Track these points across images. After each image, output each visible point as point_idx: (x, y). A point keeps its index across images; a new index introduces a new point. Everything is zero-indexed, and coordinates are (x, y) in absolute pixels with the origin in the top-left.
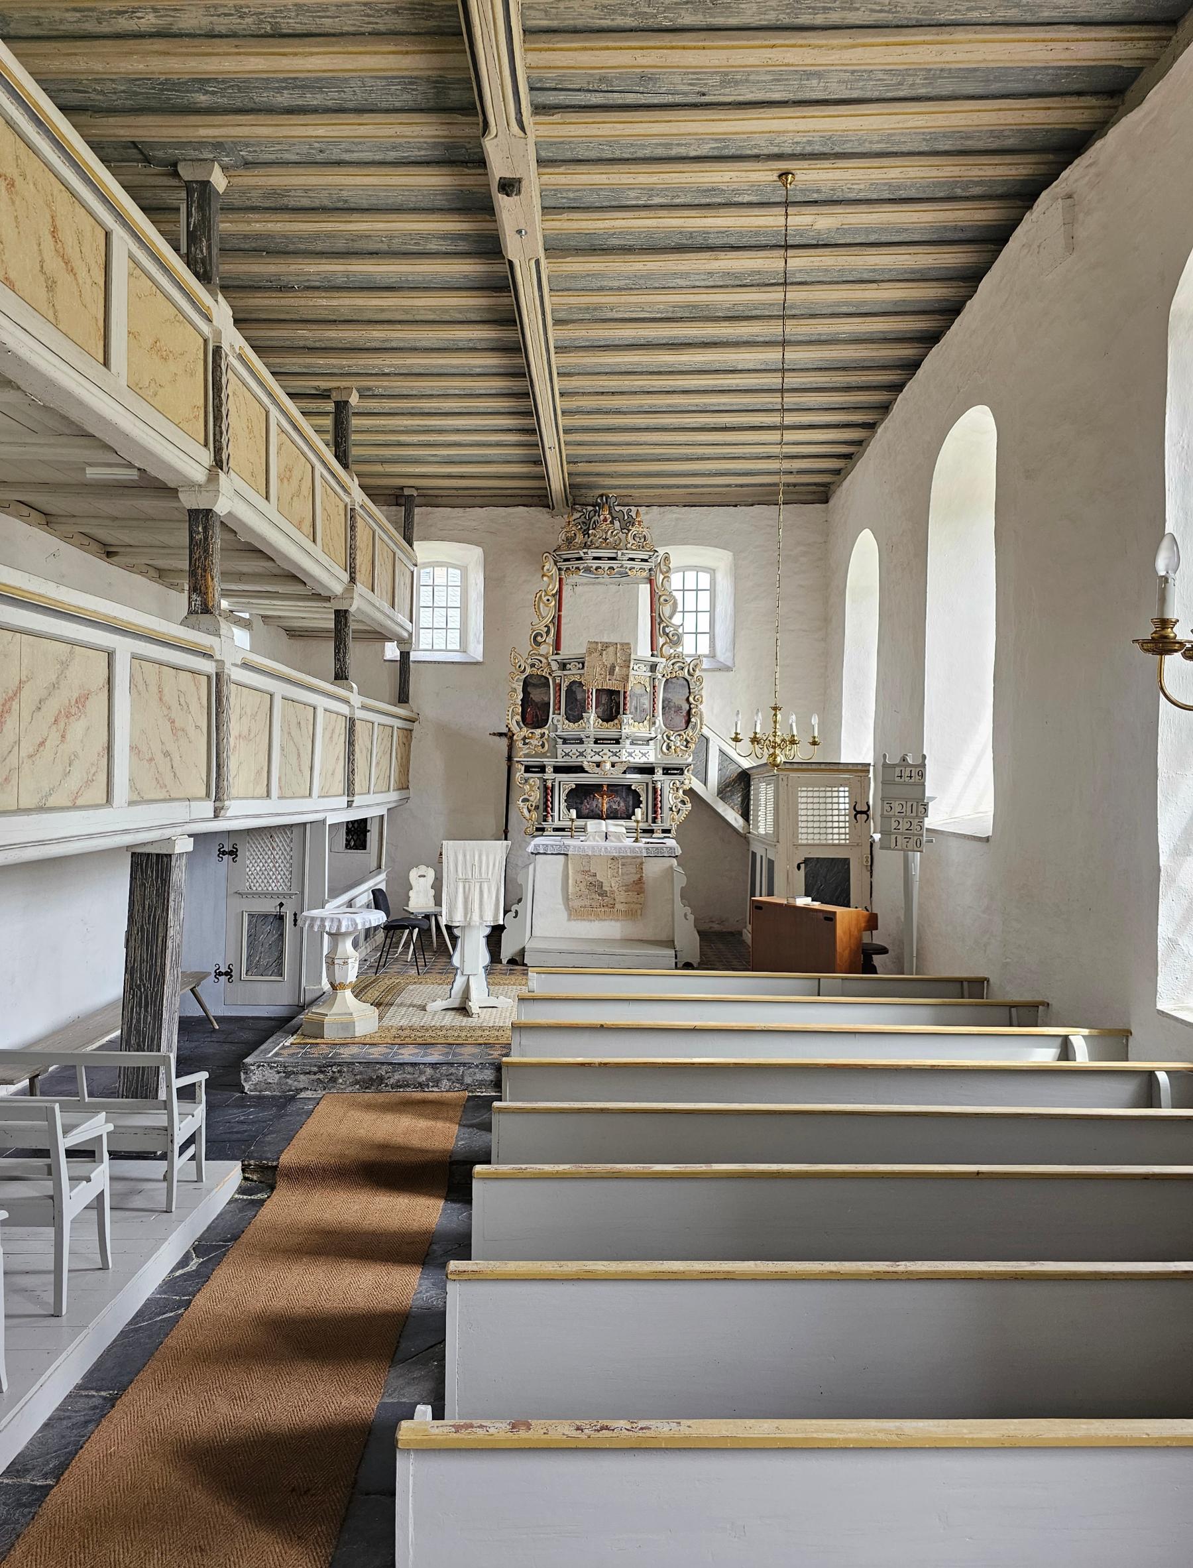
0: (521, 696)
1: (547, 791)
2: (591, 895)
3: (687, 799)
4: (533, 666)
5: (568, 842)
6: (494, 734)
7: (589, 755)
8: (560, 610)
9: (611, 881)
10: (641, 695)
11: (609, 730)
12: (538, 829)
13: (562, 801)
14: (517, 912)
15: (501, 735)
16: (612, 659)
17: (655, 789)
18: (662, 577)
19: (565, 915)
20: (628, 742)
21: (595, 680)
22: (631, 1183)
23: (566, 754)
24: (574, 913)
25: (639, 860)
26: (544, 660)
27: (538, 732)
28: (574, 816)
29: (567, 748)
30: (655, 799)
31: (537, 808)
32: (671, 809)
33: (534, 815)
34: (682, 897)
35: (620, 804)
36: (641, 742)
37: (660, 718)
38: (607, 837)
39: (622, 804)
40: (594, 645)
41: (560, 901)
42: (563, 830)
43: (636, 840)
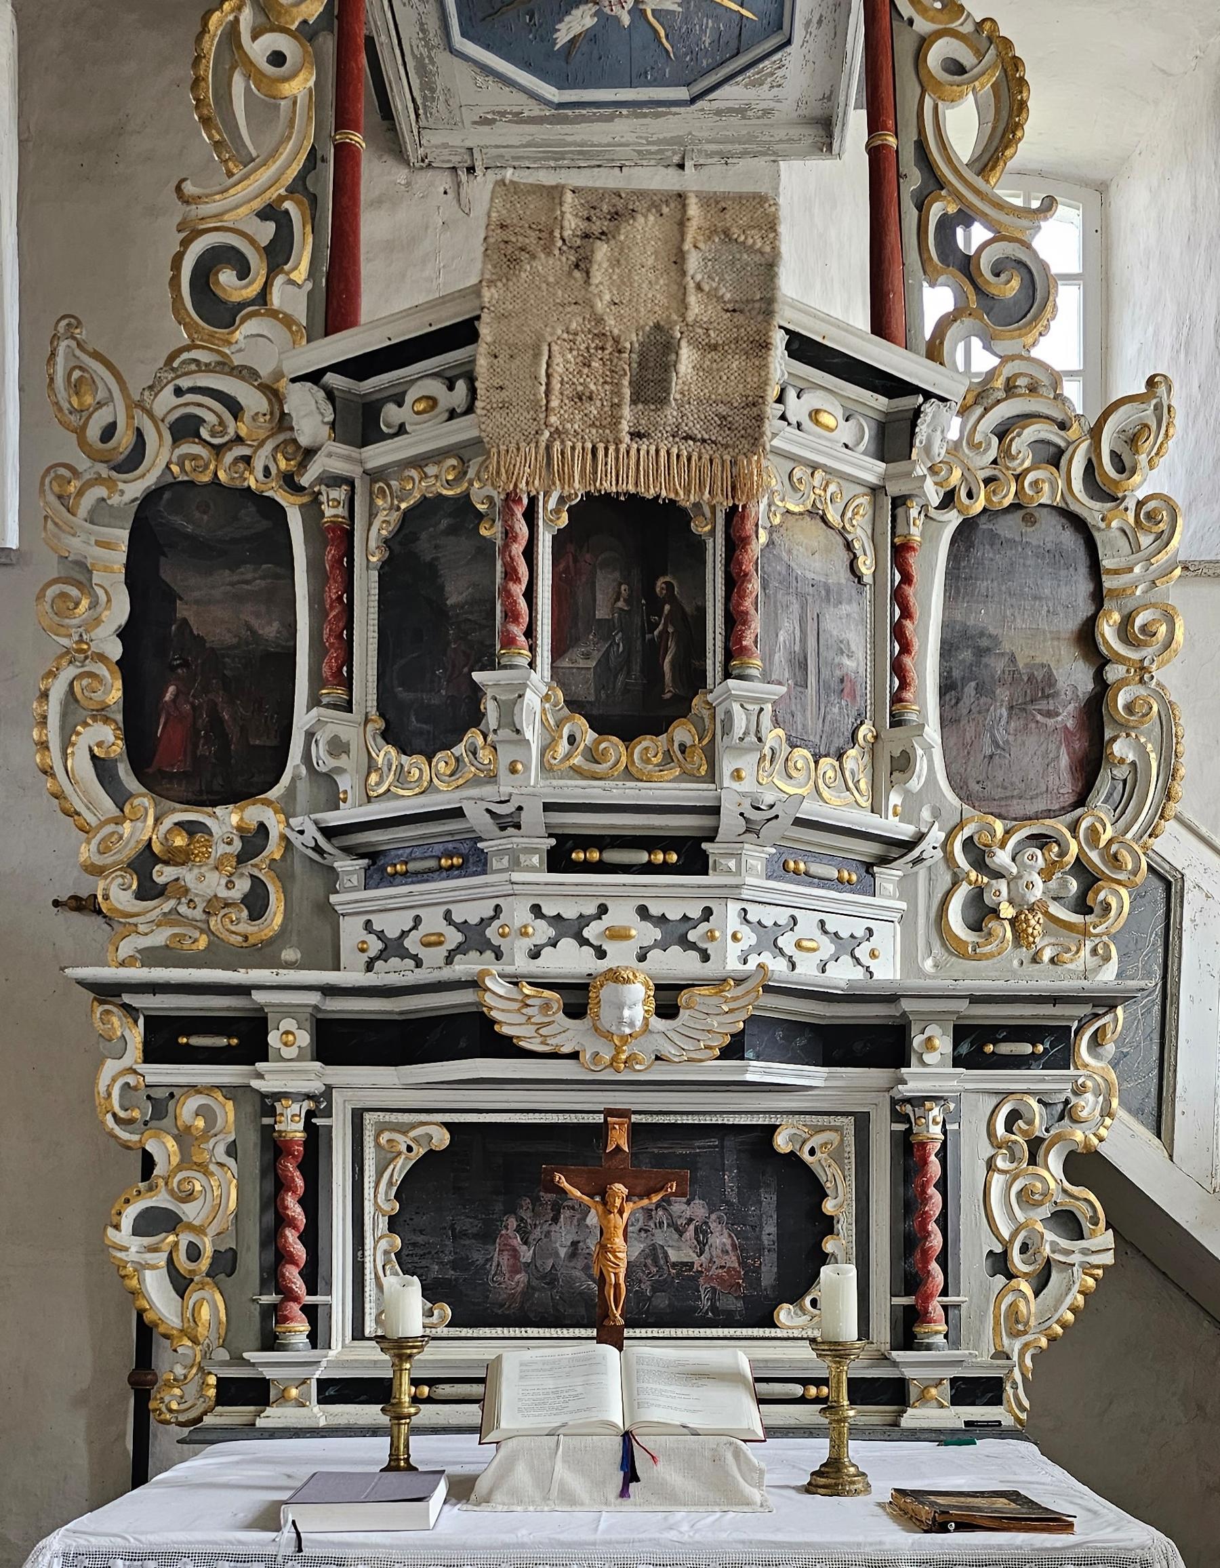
0: (120, 610)
1: (288, 1168)
3: (1086, 1201)
7: (523, 931)
10: (829, 594)
11: (642, 783)
13: (376, 1224)
16: (650, 295)
17: (908, 1150)
20: (756, 857)
21: (547, 442)
22: (397, 912)
23: (389, 936)
26: (252, 400)
27: (226, 821)
29: (395, 908)
30: (908, 1206)
31: (225, 1264)
33: (210, 1307)
35: (707, 1243)
36: (823, 867)
37: (932, 732)
39: (720, 1238)
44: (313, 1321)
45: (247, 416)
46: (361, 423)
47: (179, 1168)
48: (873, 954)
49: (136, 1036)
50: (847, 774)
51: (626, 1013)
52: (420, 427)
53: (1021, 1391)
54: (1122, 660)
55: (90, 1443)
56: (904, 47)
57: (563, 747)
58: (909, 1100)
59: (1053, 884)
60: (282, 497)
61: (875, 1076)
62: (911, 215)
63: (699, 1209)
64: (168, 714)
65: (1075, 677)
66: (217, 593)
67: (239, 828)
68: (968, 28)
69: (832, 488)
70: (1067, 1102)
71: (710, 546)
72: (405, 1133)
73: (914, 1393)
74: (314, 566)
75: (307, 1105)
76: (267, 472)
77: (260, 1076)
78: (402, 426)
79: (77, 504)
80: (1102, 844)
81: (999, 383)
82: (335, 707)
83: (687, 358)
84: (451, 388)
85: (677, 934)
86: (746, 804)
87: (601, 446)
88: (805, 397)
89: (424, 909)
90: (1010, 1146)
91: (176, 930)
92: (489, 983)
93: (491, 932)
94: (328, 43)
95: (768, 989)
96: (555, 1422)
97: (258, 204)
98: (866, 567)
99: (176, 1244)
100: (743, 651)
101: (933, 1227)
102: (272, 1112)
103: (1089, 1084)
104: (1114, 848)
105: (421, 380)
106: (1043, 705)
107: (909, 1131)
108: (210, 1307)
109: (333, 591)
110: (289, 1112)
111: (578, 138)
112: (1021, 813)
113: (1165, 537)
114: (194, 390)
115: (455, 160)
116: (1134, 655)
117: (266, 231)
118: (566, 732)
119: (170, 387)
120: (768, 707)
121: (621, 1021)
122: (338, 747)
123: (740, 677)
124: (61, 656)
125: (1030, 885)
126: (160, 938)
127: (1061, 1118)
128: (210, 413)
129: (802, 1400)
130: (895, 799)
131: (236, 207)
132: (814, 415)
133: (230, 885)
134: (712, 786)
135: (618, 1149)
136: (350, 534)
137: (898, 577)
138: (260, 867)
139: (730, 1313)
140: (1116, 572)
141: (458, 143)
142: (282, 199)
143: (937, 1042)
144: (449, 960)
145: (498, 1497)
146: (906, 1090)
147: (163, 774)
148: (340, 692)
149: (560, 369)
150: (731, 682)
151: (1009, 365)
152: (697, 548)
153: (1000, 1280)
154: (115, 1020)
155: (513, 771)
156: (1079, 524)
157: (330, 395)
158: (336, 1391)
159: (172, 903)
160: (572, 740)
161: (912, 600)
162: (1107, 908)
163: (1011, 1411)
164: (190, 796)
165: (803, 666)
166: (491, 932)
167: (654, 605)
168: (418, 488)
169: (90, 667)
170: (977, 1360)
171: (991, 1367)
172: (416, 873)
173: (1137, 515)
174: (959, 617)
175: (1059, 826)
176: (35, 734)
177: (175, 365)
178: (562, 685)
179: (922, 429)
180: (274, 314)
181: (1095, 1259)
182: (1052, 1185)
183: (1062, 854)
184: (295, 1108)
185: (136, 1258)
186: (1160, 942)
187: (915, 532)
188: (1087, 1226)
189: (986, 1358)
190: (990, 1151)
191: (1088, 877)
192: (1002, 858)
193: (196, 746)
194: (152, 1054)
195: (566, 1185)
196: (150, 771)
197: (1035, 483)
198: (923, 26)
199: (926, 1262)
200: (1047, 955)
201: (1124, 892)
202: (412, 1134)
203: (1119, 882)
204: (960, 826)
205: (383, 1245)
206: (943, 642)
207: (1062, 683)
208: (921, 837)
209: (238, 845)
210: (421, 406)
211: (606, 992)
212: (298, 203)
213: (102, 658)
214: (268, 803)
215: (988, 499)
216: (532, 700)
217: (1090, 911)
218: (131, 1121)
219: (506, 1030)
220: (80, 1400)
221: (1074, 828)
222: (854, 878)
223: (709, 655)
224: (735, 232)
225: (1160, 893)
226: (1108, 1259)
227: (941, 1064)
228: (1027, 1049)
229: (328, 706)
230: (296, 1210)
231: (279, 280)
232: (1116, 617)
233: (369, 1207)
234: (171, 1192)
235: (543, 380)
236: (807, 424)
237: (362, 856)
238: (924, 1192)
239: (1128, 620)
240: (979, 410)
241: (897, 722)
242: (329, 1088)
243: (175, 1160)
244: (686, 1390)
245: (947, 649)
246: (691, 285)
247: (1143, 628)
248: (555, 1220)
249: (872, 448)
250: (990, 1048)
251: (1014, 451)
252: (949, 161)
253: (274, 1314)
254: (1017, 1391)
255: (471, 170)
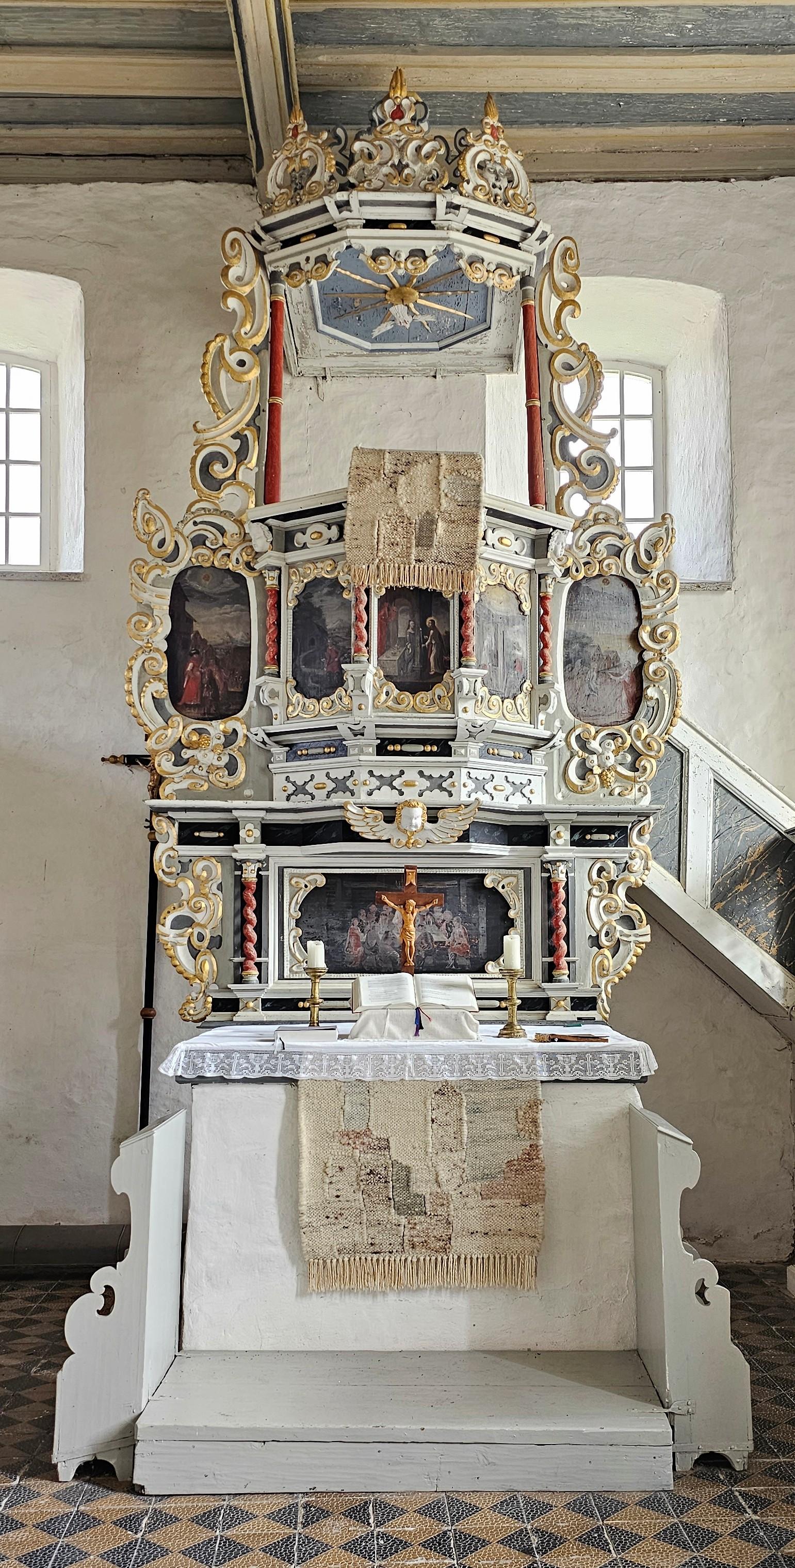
0: (166, 627)
1: (247, 895)
2: (373, 1216)
4: (198, 541)
5: (297, 1040)
6: (114, 760)
7: (363, 785)
8: (275, 390)
9: (438, 1165)
10: (508, 621)
11: (419, 715)
12: (220, 1005)
14: (109, 1294)
15: (131, 760)
17: (550, 887)
18: (556, 302)
19: (289, 1277)
20: (474, 748)
21: (375, 560)
23: (302, 788)
24: (321, 1272)
25: (524, 1096)
27: (217, 728)
28: (320, 962)
29: (300, 771)
30: (550, 913)
31: (216, 942)
32: (595, 941)
33: (209, 964)
34: (688, 1237)
36: (509, 748)
37: (560, 686)
38: (419, 1026)
39: (458, 930)
40: (372, 460)
41: (274, 1232)
42: (290, 1004)
43: (509, 1031)
44: (260, 970)
45: (228, 535)
46: (286, 542)
47: (194, 896)
48: (532, 792)
49: (174, 832)
50: (519, 707)
51: (414, 821)
52: (314, 544)
53: (605, 1004)
54: (652, 649)
55: (118, 1048)
56: (544, 358)
57: (383, 697)
58: (549, 862)
59: (619, 757)
60: (245, 573)
61: (535, 850)
62: (547, 437)
63: (448, 915)
64: (189, 677)
65: (629, 657)
66: (213, 619)
67: (224, 732)
68: (575, 348)
69: (510, 572)
70: (627, 863)
71: (451, 603)
72: (304, 878)
73: (553, 1004)
74: (261, 606)
75: (259, 865)
76: (238, 561)
77: (236, 851)
78: (305, 544)
79: (146, 577)
80: (643, 738)
81: (591, 517)
82: (272, 675)
83: (441, 526)
84: (329, 528)
85: (438, 784)
86: (470, 725)
87: (402, 566)
88: (496, 532)
89: (318, 772)
90: (599, 885)
91: (193, 781)
92: (349, 807)
93: (349, 783)
94: (266, 355)
95: (479, 809)
96: (386, 1003)
97: (232, 432)
98: (526, 607)
99: (192, 933)
100: (467, 653)
101: (562, 923)
102: (240, 868)
103: (637, 854)
104: (648, 740)
105: (314, 525)
106: (613, 671)
107: (550, 877)
108: (209, 964)
109: (271, 619)
110: (250, 869)
111: (381, 364)
112: (603, 724)
113: (671, 591)
114: (202, 523)
115: (316, 373)
116: (657, 647)
117: (236, 445)
118: (384, 691)
119: (192, 521)
120: (479, 680)
121: (411, 825)
122: (274, 694)
123: (466, 666)
124: (138, 650)
125: (608, 758)
126: (184, 785)
127: (624, 871)
128: (211, 534)
129: (499, 1008)
130: (542, 717)
131: (222, 436)
132: (500, 540)
133: (219, 759)
134: (453, 716)
135: (411, 884)
136: (279, 593)
137: (542, 612)
138: (234, 750)
139: (463, 966)
140: (648, 608)
141: (318, 365)
142: (243, 430)
143: (562, 834)
144: (328, 796)
145: (361, 1035)
146: (547, 857)
147: (186, 705)
148: (274, 668)
149: (384, 532)
150: (462, 669)
151: (596, 508)
152: (446, 604)
153: (595, 949)
154: (164, 824)
155: (360, 709)
156: (630, 584)
157: (270, 529)
158: (272, 1004)
159: (191, 767)
160: (387, 694)
161: (549, 623)
162: (645, 769)
163: (601, 1013)
164: (200, 716)
165: (496, 656)
166: (349, 783)
167: (426, 631)
168: (313, 573)
169: (152, 655)
170: (584, 989)
171: (590, 991)
172: (312, 755)
173: (657, 580)
174: (572, 628)
175: (622, 729)
176: (126, 687)
177: (193, 510)
178: (383, 668)
179: (552, 544)
180: (239, 483)
181: (641, 939)
182: (620, 903)
183: (623, 743)
184: (252, 867)
185: (173, 940)
186: (678, 783)
187: (550, 590)
188: (637, 923)
189: (588, 987)
190: (590, 887)
191: (637, 754)
192: (594, 745)
193: (202, 692)
194: (182, 841)
195: (387, 901)
196: (180, 704)
197: (608, 565)
198: (552, 348)
199: (558, 940)
200: (617, 791)
201: (653, 761)
202: (307, 879)
203: (651, 756)
204: (574, 729)
205: (293, 933)
206: (565, 641)
207: (623, 660)
208: (554, 736)
209: (223, 739)
210: (314, 536)
211: (404, 811)
212: (251, 431)
213: (158, 650)
214: (238, 719)
215: (586, 573)
216: (369, 677)
217: (638, 770)
218: (171, 873)
219: (356, 829)
220: (112, 1026)
221: (629, 730)
222: (522, 756)
223: (452, 654)
224: (462, 471)
225: (678, 759)
226: (648, 939)
227: (565, 845)
228: (607, 837)
229: (269, 675)
230: (253, 916)
231: (242, 468)
232: (648, 629)
233: (286, 915)
234: (191, 908)
235: (376, 536)
236: (497, 544)
237: (285, 746)
238: (557, 906)
239: (654, 630)
240: (581, 530)
241: (541, 681)
242: (268, 857)
243: (192, 892)
244: (444, 991)
245: (567, 644)
246: (443, 494)
247: (661, 634)
248: (377, 920)
249: (529, 552)
250: (588, 837)
251: (598, 550)
252: (566, 412)
253: (241, 966)
254: (603, 1004)
255: (324, 378)
